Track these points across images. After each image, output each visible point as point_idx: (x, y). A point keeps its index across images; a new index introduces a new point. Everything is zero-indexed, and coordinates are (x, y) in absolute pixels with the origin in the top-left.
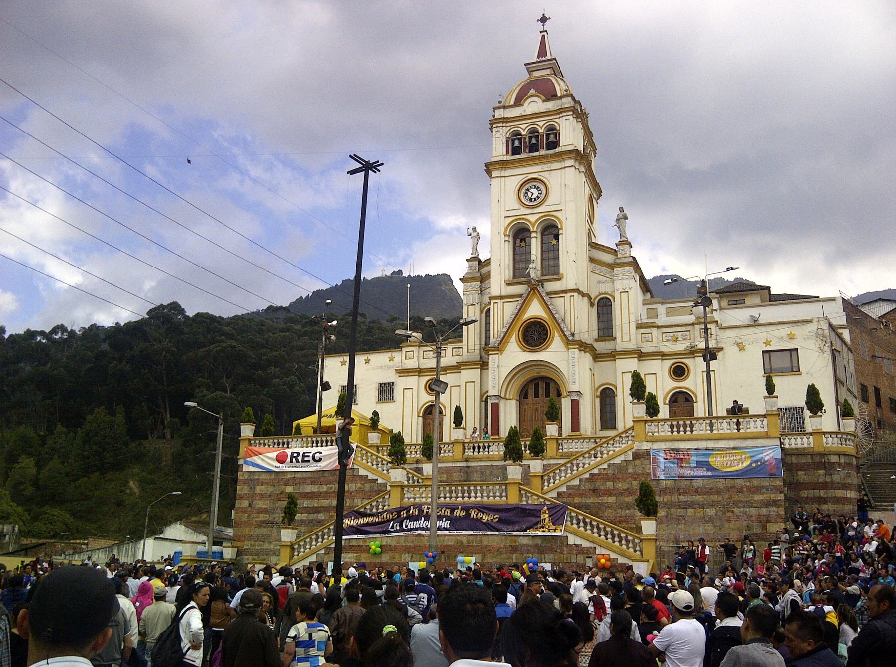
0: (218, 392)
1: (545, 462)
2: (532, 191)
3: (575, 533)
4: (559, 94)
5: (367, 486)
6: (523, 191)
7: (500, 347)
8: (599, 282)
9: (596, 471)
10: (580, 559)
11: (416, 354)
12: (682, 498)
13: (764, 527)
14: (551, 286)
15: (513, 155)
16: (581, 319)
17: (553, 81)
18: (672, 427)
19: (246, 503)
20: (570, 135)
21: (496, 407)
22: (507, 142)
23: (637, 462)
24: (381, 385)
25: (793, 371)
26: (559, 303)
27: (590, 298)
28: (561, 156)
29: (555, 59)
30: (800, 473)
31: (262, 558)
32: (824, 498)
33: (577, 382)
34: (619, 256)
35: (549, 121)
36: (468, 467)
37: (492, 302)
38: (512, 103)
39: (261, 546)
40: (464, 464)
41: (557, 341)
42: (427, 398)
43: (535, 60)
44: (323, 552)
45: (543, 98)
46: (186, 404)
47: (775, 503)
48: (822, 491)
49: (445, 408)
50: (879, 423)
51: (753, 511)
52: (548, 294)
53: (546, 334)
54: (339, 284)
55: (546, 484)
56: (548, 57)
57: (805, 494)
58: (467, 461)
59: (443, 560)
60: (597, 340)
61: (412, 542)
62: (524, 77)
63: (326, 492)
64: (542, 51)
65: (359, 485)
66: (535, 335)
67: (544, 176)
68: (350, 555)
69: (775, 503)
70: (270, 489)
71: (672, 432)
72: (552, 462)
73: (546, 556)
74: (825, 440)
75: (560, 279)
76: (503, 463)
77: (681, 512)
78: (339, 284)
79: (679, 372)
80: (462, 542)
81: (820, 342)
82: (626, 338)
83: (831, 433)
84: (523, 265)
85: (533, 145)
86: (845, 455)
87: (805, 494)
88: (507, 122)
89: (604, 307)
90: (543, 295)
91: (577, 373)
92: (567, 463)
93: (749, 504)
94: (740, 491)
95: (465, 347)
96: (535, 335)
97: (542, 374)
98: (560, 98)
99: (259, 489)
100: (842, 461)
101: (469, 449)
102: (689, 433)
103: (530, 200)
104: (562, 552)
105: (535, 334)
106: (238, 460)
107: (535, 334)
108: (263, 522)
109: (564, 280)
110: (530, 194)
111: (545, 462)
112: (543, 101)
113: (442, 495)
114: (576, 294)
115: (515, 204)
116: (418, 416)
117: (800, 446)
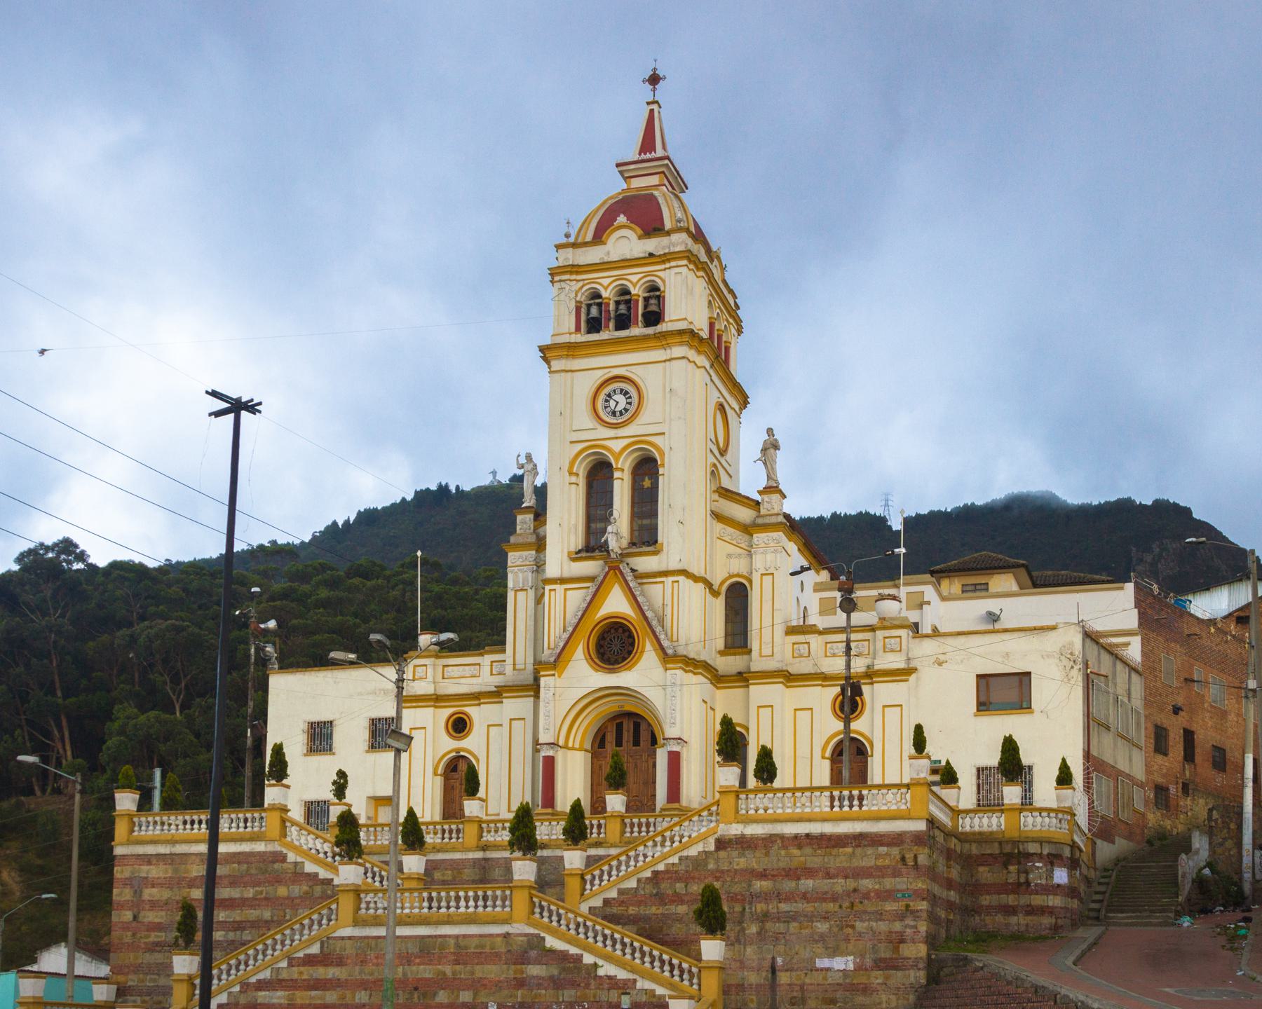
0: (152, 714)
1: (593, 852)
2: (618, 400)
3: (609, 958)
4: (668, 225)
5: (318, 890)
6: (602, 397)
7: (558, 662)
9: (661, 867)
10: (614, 996)
11: (430, 670)
12: (784, 907)
13: (896, 949)
14: (646, 563)
15: (589, 332)
16: (694, 619)
17: (661, 200)
18: (832, 798)
19: (128, 916)
20: (686, 302)
21: (550, 763)
22: (578, 309)
23: (722, 854)
25: (1022, 708)
26: (656, 592)
27: (709, 585)
28: (664, 339)
29: (668, 158)
30: (981, 869)
31: (155, 998)
32: (1013, 907)
33: (678, 721)
34: (763, 512)
35: (648, 274)
36: (486, 860)
37: (547, 588)
38: (589, 238)
39: (155, 980)
40: (479, 855)
41: (648, 659)
42: (448, 744)
43: (636, 157)
44: (237, 988)
45: (640, 231)
46: (20, 758)
47: (915, 914)
48: (1011, 897)
49: (478, 760)
50: (1185, 788)
51: (882, 926)
53: (633, 644)
54: (409, 498)
55: (588, 886)
56: (659, 152)
57: (986, 900)
58: (484, 848)
59: (416, 1000)
61: (372, 974)
62: (615, 186)
63: (254, 899)
64: (648, 143)
65: (305, 888)
66: (616, 646)
67: (636, 374)
68: (279, 993)
70: (166, 894)
71: (832, 807)
72: (600, 851)
73: (566, 992)
74: (1022, 819)
75: (656, 553)
76: (506, 854)
77: (781, 927)
78: (409, 498)
79: (459, 726)
80: (444, 974)
81: (1065, 662)
83: (1049, 810)
84: (600, 525)
85: (621, 316)
86: (1049, 842)
87: (986, 900)
88: (577, 273)
89: (737, 599)
91: (678, 709)
92: (621, 854)
93: (880, 916)
94: (866, 896)
95: (509, 661)
96: (616, 646)
97: (628, 708)
98: (668, 233)
99: (148, 893)
100: (1045, 852)
101: (489, 832)
102: (856, 808)
103: (614, 413)
104: (587, 986)
105: (614, 644)
106: (112, 848)
107: (614, 644)
108: (157, 944)
109: (663, 556)
110: (612, 404)
111: (593, 852)
112: (640, 238)
113: (399, 905)
114: (681, 578)
115: (587, 421)
116: (435, 774)
117: (985, 829)
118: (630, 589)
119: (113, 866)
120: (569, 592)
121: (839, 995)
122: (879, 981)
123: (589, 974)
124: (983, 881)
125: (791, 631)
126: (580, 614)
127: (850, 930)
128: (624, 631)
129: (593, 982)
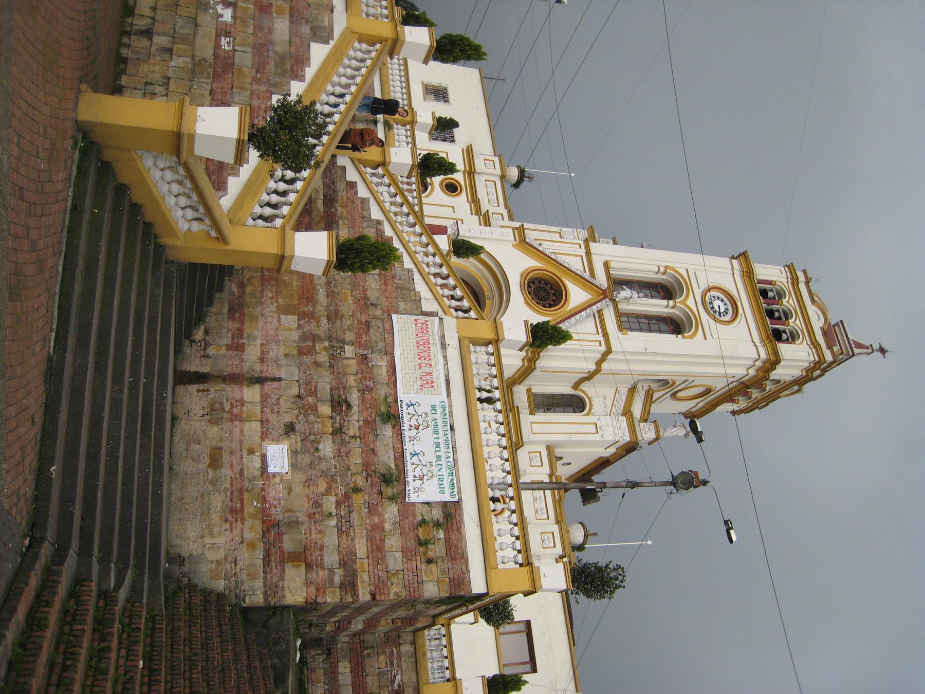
8: (605, 398)
24: (454, 141)
27: (590, 376)
51: (331, 539)
52: (600, 312)
57: (344, 668)
60: (529, 391)
69: (350, 585)
82: (536, 428)
87: (344, 668)
88: (793, 284)
90: (599, 305)
104: (256, 81)
118: (591, 306)
119: (189, 372)
120: (579, 259)
121: (226, 472)
122: (247, 535)
123: (275, 85)
124: (368, 662)
125: (549, 449)
126: (566, 265)
127: (322, 486)
128: (554, 301)
129: (263, 88)
